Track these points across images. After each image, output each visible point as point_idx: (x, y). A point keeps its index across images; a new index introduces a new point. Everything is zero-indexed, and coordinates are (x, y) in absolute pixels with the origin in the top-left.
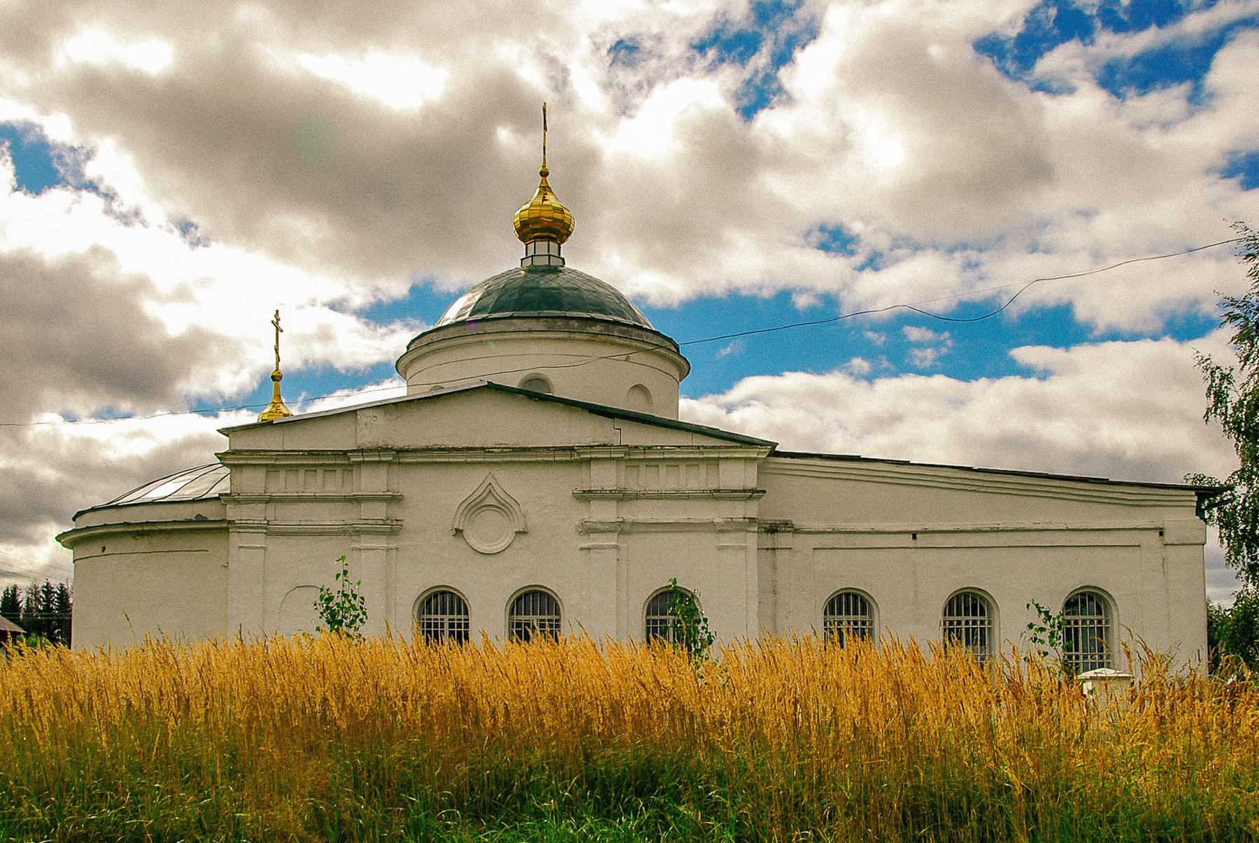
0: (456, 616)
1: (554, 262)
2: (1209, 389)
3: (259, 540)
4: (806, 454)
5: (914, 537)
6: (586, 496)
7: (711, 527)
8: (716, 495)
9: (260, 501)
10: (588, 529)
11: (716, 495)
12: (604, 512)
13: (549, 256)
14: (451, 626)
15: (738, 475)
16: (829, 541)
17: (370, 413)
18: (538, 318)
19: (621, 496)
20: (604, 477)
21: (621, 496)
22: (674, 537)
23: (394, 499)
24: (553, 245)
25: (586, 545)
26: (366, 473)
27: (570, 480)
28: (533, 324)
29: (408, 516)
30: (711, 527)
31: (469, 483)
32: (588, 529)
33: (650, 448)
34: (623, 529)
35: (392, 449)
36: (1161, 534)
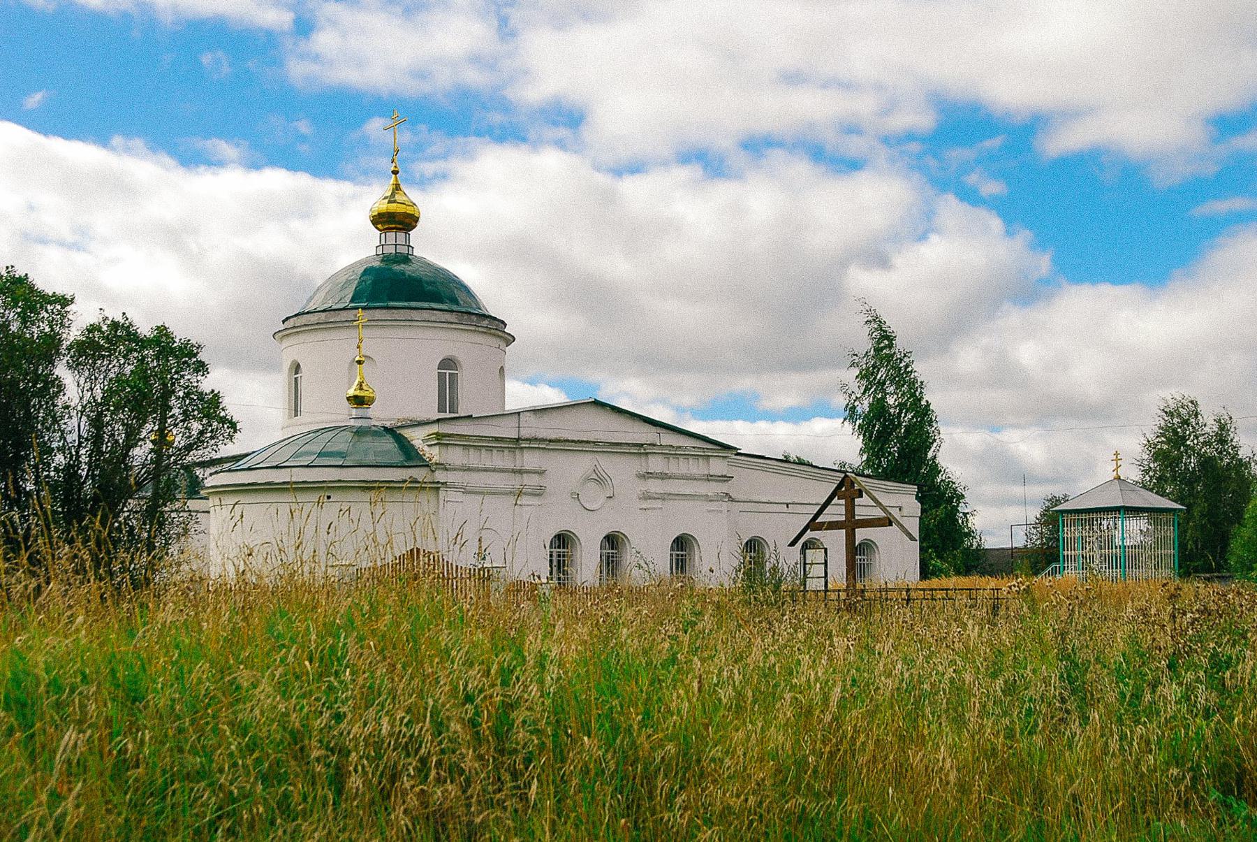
0: (562, 550)
1: (404, 250)
2: (847, 407)
3: (459, 497)
4: (1150, 508)
5: (788, 507)
6: (647, 476)
7: (708, 499)
8: (709, 478)
9: (461, 470)
10: (646, 497)
11: (709, 478)
12: (655, 486)
13: (396, 245)
14: (559, 556)
15: (718, 466)
16: (748, 506)
17: (528, 414)
18: (452, 311)
19: (664, 477)
20: (656, 464)
21: (664, 477)
22: (685, 503)
23: (541, 473)
24: (401, 235)
25: (643, 506)
26: (526, 454)
27: (634, 465)
28: (448, 317)
29: (548, 482)
30: (708, 499)
31: (582, 464)
32: (646, 497)
33: (680, 447)
34: (664, 497)
35: (546, 440)
36: (900, 510)
